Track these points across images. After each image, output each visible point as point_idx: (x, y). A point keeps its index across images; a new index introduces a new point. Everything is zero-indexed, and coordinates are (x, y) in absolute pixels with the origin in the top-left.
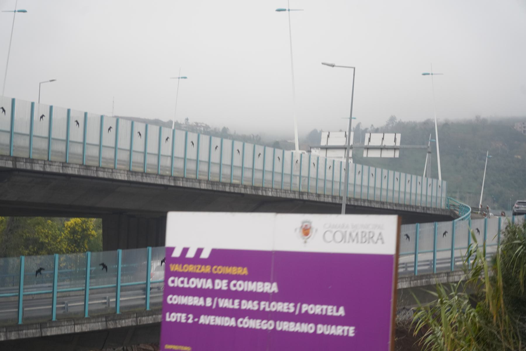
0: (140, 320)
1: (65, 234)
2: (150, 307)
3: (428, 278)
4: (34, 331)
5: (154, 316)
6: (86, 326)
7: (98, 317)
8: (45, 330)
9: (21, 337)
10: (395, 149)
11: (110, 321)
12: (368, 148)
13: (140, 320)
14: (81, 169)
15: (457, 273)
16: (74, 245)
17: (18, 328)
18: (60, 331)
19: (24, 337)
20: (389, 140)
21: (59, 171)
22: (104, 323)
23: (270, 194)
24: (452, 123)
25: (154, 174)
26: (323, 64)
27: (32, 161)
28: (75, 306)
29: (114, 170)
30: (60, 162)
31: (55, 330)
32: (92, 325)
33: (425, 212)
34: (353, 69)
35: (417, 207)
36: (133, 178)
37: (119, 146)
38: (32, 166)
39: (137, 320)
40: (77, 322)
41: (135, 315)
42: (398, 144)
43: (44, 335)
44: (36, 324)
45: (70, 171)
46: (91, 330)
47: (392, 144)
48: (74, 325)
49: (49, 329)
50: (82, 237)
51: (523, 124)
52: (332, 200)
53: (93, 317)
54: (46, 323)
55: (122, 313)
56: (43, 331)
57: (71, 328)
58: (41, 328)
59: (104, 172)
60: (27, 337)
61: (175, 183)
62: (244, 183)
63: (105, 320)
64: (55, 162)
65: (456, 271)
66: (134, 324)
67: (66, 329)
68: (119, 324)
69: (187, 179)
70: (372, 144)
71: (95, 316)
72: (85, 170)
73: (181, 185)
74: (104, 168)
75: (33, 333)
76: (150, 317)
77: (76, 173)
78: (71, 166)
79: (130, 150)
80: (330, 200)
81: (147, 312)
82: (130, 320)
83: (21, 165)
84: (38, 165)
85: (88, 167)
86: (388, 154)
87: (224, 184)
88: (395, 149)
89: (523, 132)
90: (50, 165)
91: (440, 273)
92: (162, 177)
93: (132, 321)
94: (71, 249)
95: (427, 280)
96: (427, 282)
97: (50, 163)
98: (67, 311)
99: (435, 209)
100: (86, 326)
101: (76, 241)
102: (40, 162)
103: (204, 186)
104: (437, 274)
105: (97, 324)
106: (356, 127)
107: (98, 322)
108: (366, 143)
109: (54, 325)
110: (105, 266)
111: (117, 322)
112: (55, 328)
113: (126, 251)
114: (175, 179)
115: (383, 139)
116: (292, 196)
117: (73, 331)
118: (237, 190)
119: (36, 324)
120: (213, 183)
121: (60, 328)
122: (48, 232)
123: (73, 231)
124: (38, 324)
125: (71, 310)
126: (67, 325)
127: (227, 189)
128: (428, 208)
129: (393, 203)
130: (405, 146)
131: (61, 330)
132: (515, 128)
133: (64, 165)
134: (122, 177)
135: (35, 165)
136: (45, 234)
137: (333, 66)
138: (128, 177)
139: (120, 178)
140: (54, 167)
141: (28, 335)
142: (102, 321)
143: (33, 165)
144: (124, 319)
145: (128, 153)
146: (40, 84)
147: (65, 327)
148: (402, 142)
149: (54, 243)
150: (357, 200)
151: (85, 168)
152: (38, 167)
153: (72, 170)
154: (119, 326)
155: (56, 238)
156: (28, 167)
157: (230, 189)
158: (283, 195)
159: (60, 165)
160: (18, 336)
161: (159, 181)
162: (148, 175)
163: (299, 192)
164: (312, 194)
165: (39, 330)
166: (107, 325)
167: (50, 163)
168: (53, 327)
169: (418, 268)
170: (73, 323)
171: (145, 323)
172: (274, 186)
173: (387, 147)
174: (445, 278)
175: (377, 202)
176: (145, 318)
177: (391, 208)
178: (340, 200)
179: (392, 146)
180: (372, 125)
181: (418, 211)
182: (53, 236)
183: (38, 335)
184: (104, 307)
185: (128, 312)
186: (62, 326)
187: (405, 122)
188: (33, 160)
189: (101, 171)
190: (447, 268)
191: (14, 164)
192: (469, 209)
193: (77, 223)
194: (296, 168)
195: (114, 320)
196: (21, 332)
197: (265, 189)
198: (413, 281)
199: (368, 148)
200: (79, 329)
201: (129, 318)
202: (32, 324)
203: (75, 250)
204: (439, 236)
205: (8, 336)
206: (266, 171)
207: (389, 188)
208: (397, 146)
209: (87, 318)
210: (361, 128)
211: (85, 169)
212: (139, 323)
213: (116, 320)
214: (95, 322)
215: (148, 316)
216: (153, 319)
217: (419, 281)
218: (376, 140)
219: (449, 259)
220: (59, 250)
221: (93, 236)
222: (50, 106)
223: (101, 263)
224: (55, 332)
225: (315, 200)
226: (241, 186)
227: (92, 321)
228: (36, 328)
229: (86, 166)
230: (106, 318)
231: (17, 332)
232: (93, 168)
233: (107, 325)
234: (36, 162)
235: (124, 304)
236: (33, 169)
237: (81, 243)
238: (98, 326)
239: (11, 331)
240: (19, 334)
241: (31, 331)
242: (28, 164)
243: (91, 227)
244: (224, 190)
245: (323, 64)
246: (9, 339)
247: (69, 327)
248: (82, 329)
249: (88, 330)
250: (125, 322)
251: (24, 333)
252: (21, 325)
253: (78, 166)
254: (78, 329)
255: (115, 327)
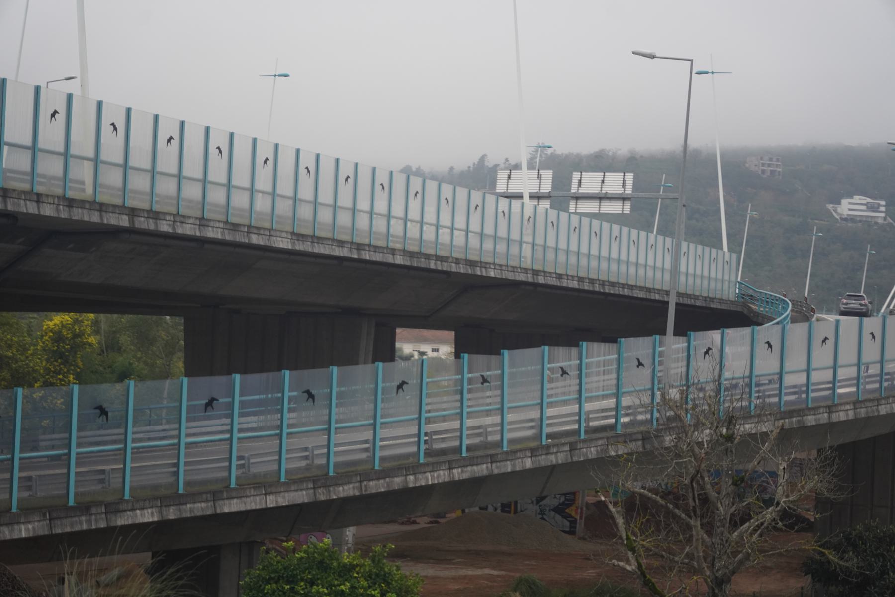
0: (366, 486)
1: (43, 343)
2: (380, 466)
3: (800, 416)
4: (203, 505)
5: (387, 479)
6: (284, 497)
7: (301, 481)
8: (221, 502)
9: (185, 515)
10: (623, 199)
11: (320, 487)
12: (578, 198)
13: (366, 486)
14: (226, 229)
15: (843, 407)
16: (59, 361)
17: (179, 500)
18: (244, 505)
19: (188, 515)
20: (614, 183)
21: (195, 233)
22: (312, 491)
23: (492, 274)
24: (642, 157)
25: (328, 239)
26: (634, 53)
27: (156, 215)
28: (262, 465)
29: (272, 233)
30: (197, 218)
31: (236, 503)
32: (292, 494)
33: (708, 306)
34: (690, 62)
35: (696, 297)
36: (300, 246)
37: (279, 191)
38: (156, 224)
39: (361, 485)
40: (269, 490)
41: (359, 478)
42: (629, 191)
43: (218, 511)
44: (207, 493)
45: (211, 233)
46: (291, 503)
47: (619, 190)
48: (265, 494)
49: (227, 502)
50: (71, 348)
51: (762, 158)
52: (579, 285)
53: (295, 482)
54: (221, 492)
55: (338, 473)
56: (217, 504)
57: (260, 500)
58: (214, 500)
59: (258, 234)
60: (193, 515)
61: (359, 254)
62: (455, 255)
63: (312, 486)
64: (189, 217)
65: (841, 404)
66: (357, 493)
67: (253, 503)
68: (335, 493)
69: (376, 248)
70: (583, 190)
71: (296, 481)
72: (231, 231)
73: (368, 258)
74: (258, 228)
75: (202, 508)
76: (382, 481)
77: (219, 236)
78: (212, 224)
79: (295, 199)
80: (574, 284)
81: (376, 472)
82: (351, 486)
83: (142, 223)
84: (164, 222)
85: (235, 227)
86: (614, 208)
87: (428, 257)
88: (623, 199)
89: (760, 173)
90: (182, 222)
91: (819, 407)
92: (341, 243)
93: (353, 488)
94: (54, 368)
95: (798, 418)
96: (798, 421)
97: (182, 219)
98: (249, 471)
99: (721, 301)
100: (284, 497)
101: (61, 355)
102: (168, 218)
103: (399, 260)
104: (813, 408)
105: (300, 493)
106: (479, 162)
107: (302, 490)
108: (574, 190)
109: (234, 494)
110: (311, 396)
111: (331, 489)
112: (235, 500)
113: (294, 372)
114: (359, 247)
115: (603, 182)
116: (521, 277)
117: (264, 506)
118: (445, 267)
119: (207, 493)
120: (411, 255)
121: (244, 499)
122: (12, 339)
123: (58, 337)
124: (209, 492)
125: (254, 470)
126: (254, 495)
127: (432, 266)
128: (712, 300)
129: (662, 290)
130: (641, 195)
131: (245, 504)
132: (747, 165)
133: (203, 222)
134: (284, 243)
135: (161, 222)
136: (6, 342)
137: (653, 57)
138: (293, 244)
139: (282, 245)
140: (188, 226)
141: (194, 512)
142: (307, 489)
143: (158, 221)
144: (342, 484)
145: (291, 202)
146: (48, 82)
147: (252, 497)
148: (635, 187)
149: (23, 358)
150: (612, 284)
151: (231, 227)
152: (164, 227)
153: (213, 231)
154: (335, 497)
155: (26, 350)
156: (150, 225)
157: (435, 264)
158: (510, 276)
159: (195, 223)
160: (179, 513)
161: (338, 252)
162: (320, 240)
163: (533, 270)
164: (550, 273)
165: (211, 503)
166: (315, 495)
167: (182, 219)
168: (233, 498)
169: (785, 398)
170: (264, 492)
171: (374, 491)
172: (497, 261)
173: (610, 196)
174: (826, 415)
175: (642, 288)
176: (374, 482)
177: (661, 299)
178: (581, 283)
179: (619, 194)
180: (507, 160)
181: (698, 303)
182: (20, 346)
183: (209, 512)
184: (303, 463)
185: (348, 471)
186: (247, 496)
187: (562, 154)
188: (157, 213)
189: (255, 233)
190: (825, 398)
191: (132, 221)
192: (788, 304)
193: (64, 323)
194: (527, 231)
195: (326, 486)
196: (184, 507)
197: (485, 265)
198: (778, 420)
199: (578, 198)
200: (273, 502)
201: (349, 483)
202: (201, 493)
203: (61, 369)
204: (761, 349)
205: (164, 513)
206: (486, 235)
207: (657, 265)
208: (627, 194)
209: (284, 483)
210: (486, 163)
211: (232, 230)
212: (365, 491)
213: (329, 486)
214: (297, 490)
215: (378, 479)
216: (386, 485)
217: (787, 420)
218: (591, 182)
219: (829, 383)
220: (31, 369)
221: (90, 345)
222: (181, 121)
223: (304, 390)
224: (235, 506)
225: (555, 284)
226: (451, 260)
227: (293, 488)
228: (207, 501)
229: (233, 224)
230: (314, 482)
231: (178, 507)
232: (242, 228)
233: (315, 495)
234: (162, 218)
235: (341, 459)
236: (159, 229)
237: (71, 358)
238: (301, 496)
239: (168, 506)
240: (180, 510)
241: (199, 505)
242: (151, 220)
243: (88, 330)
244: (428, 267)
245: (634, 53)
246: (165, 518)
247: (258, 498)
248: (277, 501)
249: (287, 503)
250: (343, 489)
251: (189, 509)
252: (182, 495)
253: (222, 225)
254: (271, 501)
255: (328, 498)
